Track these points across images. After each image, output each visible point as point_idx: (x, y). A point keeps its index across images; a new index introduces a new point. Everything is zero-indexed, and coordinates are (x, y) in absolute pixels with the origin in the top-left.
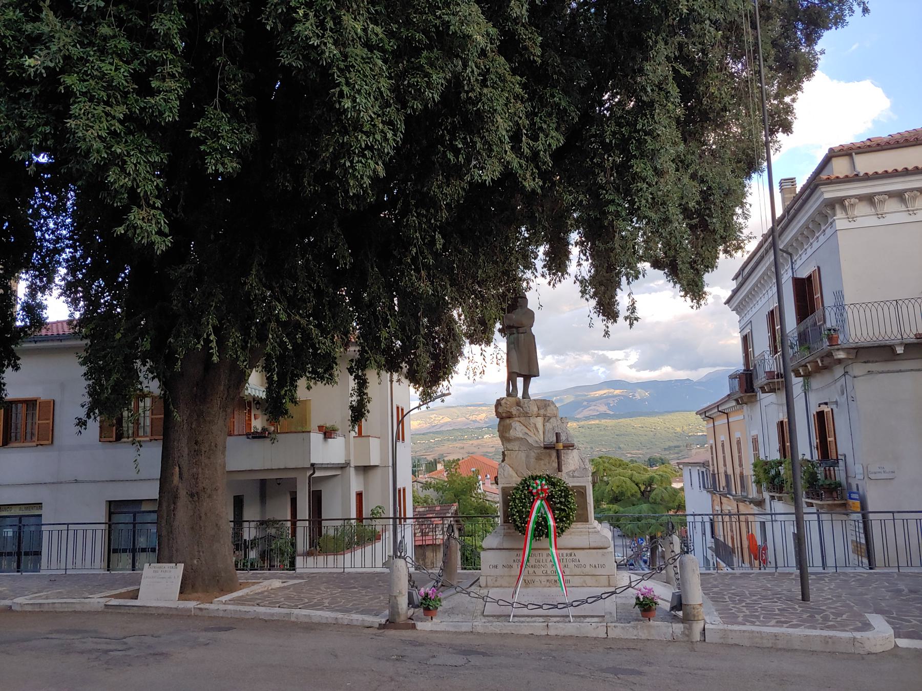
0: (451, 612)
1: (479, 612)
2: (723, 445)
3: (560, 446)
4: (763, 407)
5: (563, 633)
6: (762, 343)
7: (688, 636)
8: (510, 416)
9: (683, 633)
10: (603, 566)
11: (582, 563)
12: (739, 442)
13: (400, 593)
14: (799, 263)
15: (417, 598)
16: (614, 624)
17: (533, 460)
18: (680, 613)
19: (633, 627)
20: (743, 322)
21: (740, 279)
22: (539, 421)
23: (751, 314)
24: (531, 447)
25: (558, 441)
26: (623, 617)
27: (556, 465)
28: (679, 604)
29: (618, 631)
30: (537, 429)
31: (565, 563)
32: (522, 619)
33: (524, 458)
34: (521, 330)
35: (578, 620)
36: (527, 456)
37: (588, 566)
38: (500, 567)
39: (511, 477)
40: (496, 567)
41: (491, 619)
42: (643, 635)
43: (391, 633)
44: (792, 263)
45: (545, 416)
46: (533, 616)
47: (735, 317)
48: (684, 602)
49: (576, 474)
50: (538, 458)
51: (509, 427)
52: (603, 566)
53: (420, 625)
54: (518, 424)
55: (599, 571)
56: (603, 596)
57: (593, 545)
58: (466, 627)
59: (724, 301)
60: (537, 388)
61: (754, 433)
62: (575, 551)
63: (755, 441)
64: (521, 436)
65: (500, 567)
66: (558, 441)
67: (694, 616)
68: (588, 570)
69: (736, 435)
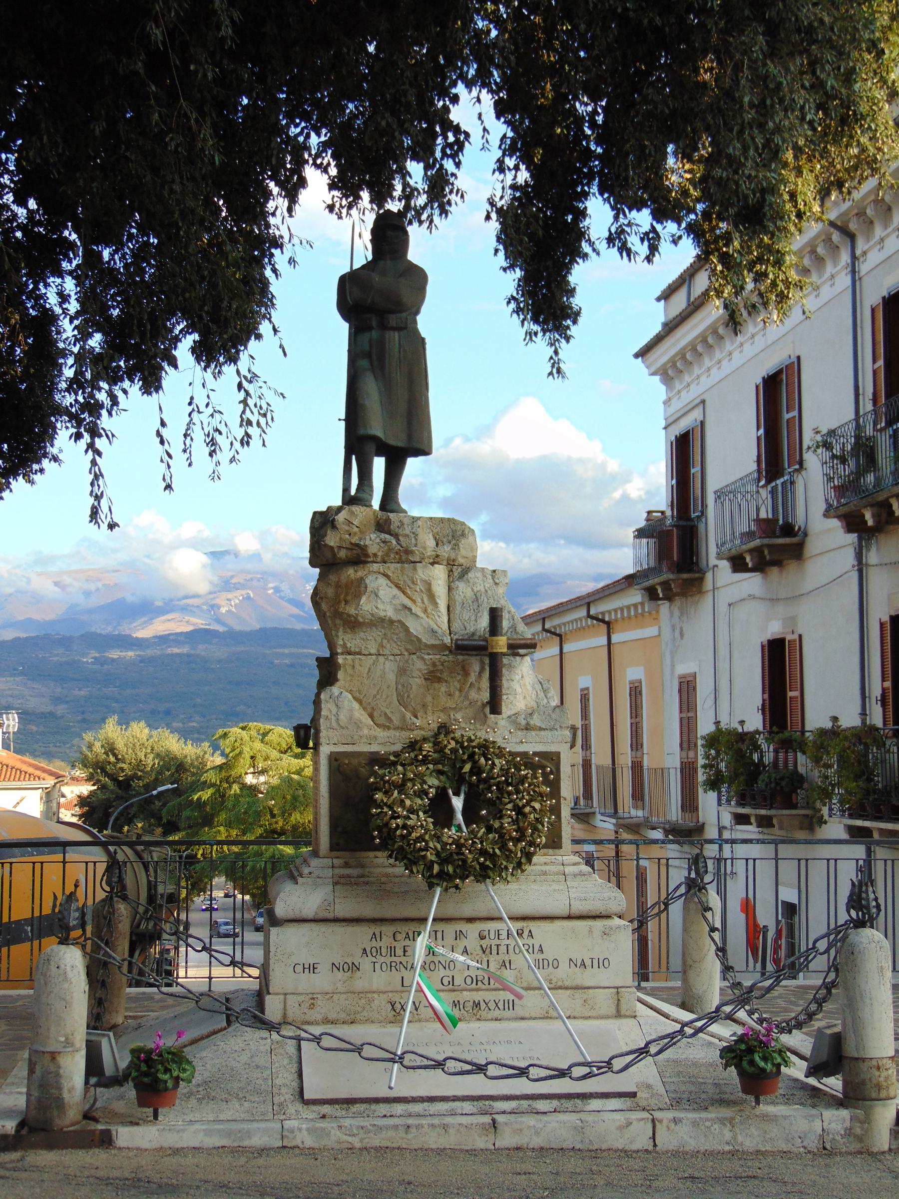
0: (209, 1093)
1: (287, 1094)
2: (585, 698)
3: (501, 644)
4: (722, 607)
5: (537, 1142)
6: (731, 455)
7: (860, 1139)
8: (359, 557)
9: (849, 1132)
10: (603, 963)
11: (549, 954)
12: (636, 691)
13: (68, 1043)
14: (874, 258)
15: (116, 1056)
16: (670, 1115)
17: (417, 682)
18: (834, 1084)
19: (722, 1121)
20: (677, 405)
21: (680, 301)
22: (439, 574)
23: (705, 382)
24: (415, 646)
25: (495, 626)
26: (692, 1096)
27: (486, 696)
28: (834, 1057)
29: (684, 1132)
30: (432, 597)
31: (503, 956)
32: (417, 1108)
33: (391, 677)
34: (393, 320)
35: (568, 1104)
36: (402, 672)
37: (564, 965)
38: (324, 968)
39: (358, 725)
40: (313, 968)
41: (326, 1109)
42: (750, 1139)
43: (45, 1158)
44: (854, 258)
45: (451, 564)
46: (584, 1096)
47: (657, 388)
48: (850, 1050)
49: (536, 721)
50: (433, 677)
51: (357, 589)
52: (603, 963)
53: (124, 1135)
54: (382, 581)
55: (588, 977)
56: (368, 1051)
57: (579, 907)
58: (262, 1135)
59: (636, 349)
60: (425, 489)
61: (684, 668)
62: (533, 926)
63: (687, 688)
64: (390, 613)
65: (324, 968)
66: (495, 626)
67: (879, 1087)
68: (564, 973)
69: (632, 672)
